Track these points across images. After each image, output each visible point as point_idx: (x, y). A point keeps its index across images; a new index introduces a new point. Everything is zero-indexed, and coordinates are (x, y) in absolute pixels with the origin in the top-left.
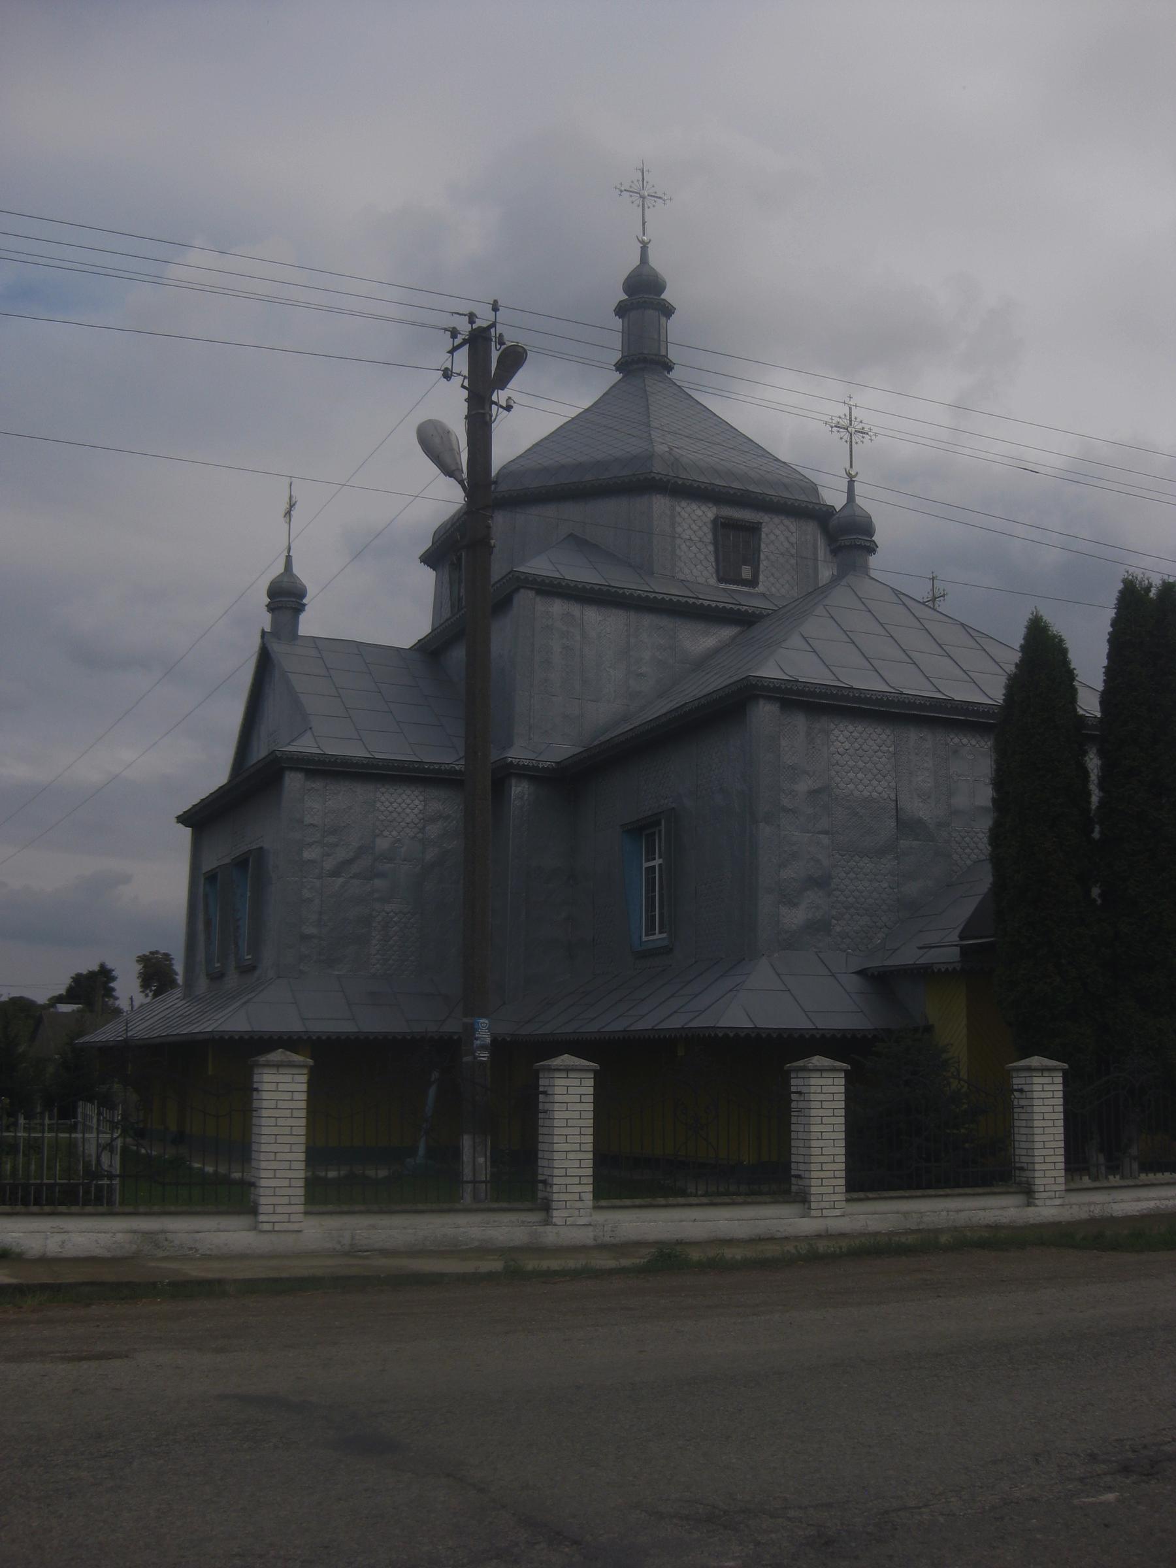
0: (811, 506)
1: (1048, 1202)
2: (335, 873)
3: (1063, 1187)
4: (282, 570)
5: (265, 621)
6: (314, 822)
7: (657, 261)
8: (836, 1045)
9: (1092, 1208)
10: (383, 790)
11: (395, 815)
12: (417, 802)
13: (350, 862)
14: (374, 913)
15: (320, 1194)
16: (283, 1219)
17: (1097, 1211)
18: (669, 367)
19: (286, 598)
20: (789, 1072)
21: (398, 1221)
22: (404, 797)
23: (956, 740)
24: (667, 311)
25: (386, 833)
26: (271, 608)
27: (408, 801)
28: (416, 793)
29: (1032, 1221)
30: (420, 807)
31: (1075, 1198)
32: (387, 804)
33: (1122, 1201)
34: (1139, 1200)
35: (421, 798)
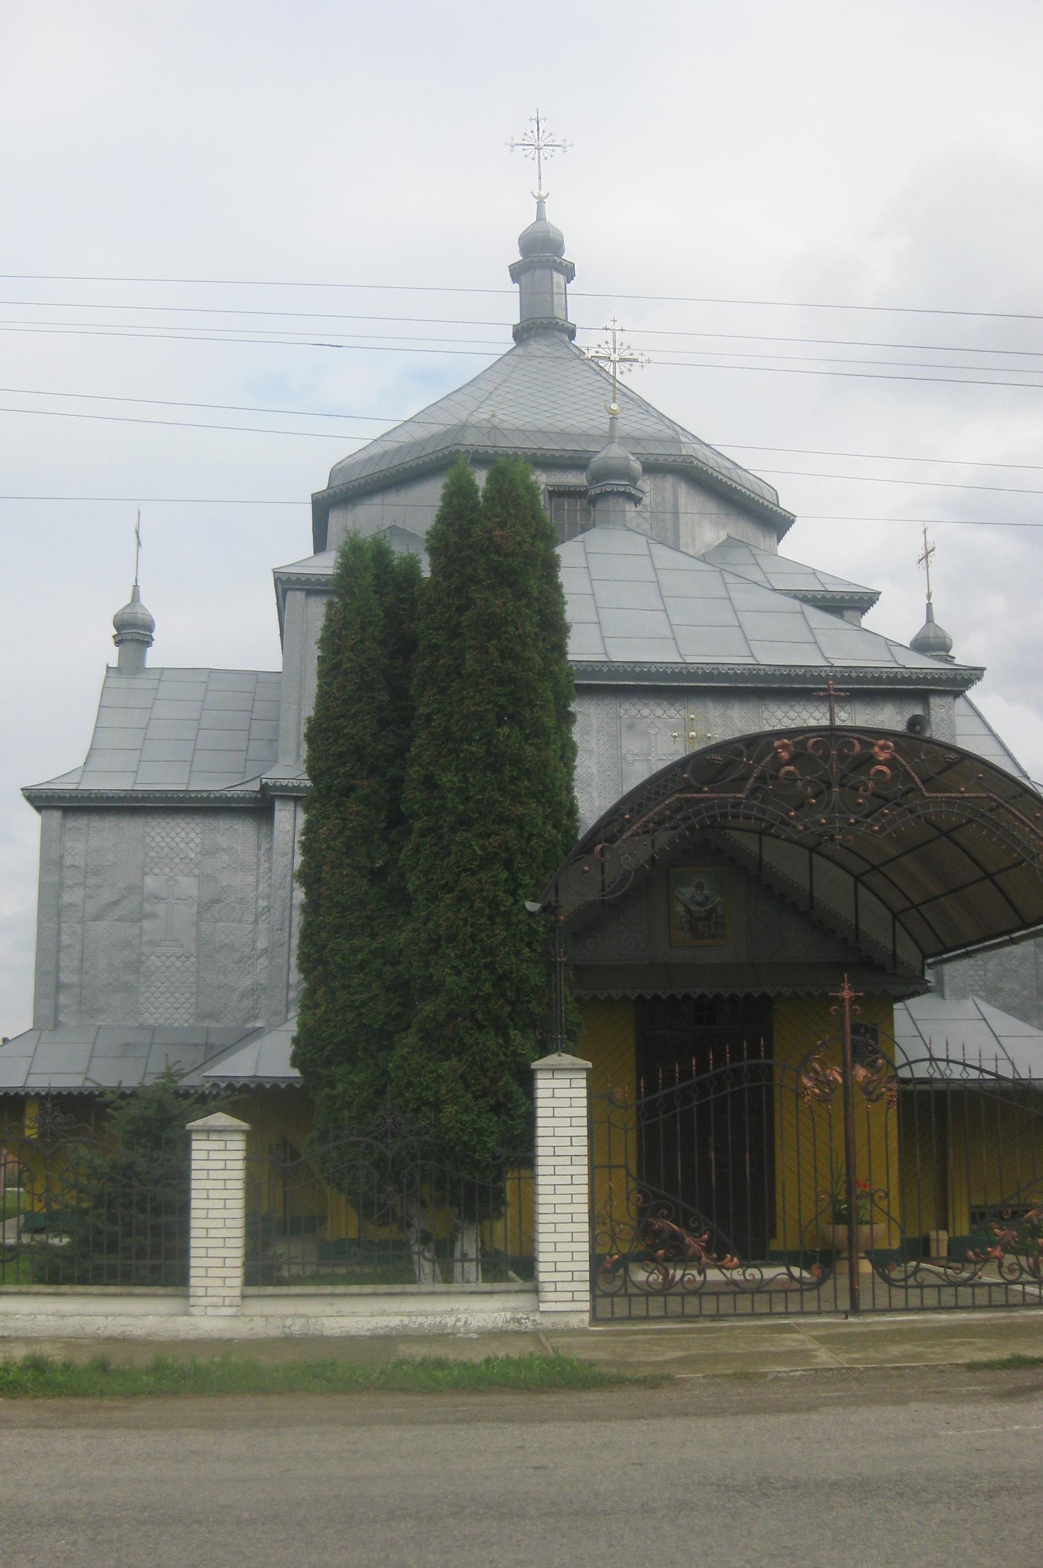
0: (661, 460)
1: (210, 1311)
2: (98, 917)
3: (237, 1292)
4: (924, 621)
5: (112, 655)
6: (76, 864)
7: (555, 218)
8: (250, 1100)
9: (288, 1322)
10: (154, 824)
11: (166, 850)
12: (193, 835)
13: (115, 903)
14: (143, 958)
15: (261, 1271)
16: (216, 1298)
17: (297, 1327)
18: (572, 334)
19: (133, 632)
20: (189, 1133)
21: (362, 1306)
22: (178, 830)
23: (633, 712)
24: (569, 272)
25: (157, 871)
26: (119, 641)
27: (183, 834)
28: (192, 825)
29: (182, 1335)
30: (198, 840)
31: (256, 1307)
32: (158, 839)
33: (354, 1314)
34: (384, 1313)
35: (198, 830)
